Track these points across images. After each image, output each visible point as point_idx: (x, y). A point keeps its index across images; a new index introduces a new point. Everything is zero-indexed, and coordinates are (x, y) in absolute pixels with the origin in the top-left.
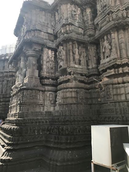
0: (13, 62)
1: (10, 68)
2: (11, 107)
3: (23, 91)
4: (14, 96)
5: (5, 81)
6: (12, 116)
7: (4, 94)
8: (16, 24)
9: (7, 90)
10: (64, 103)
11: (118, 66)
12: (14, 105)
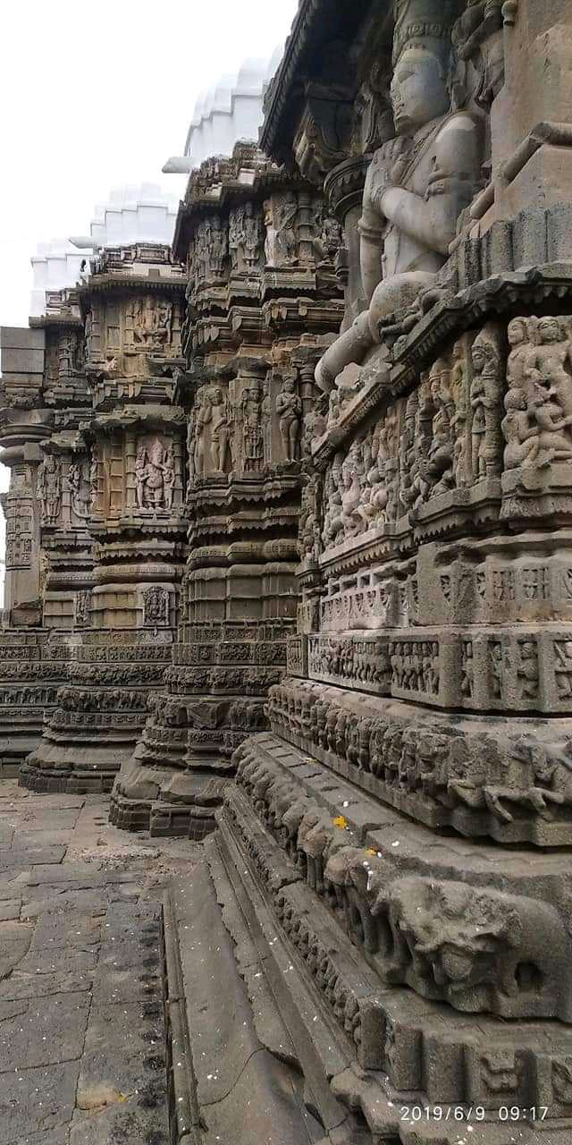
0: (307, 118)
1: (271, 264)
2: (317, 571)
3: (484, 338)
4: (338, 449)
5: (243, 372)
6: (337, 669)
7: (240, 477)
8: (286, 31)
9: (260, 445)
10: (227, 466)
11: (139, 535)
12: (349, 543)
